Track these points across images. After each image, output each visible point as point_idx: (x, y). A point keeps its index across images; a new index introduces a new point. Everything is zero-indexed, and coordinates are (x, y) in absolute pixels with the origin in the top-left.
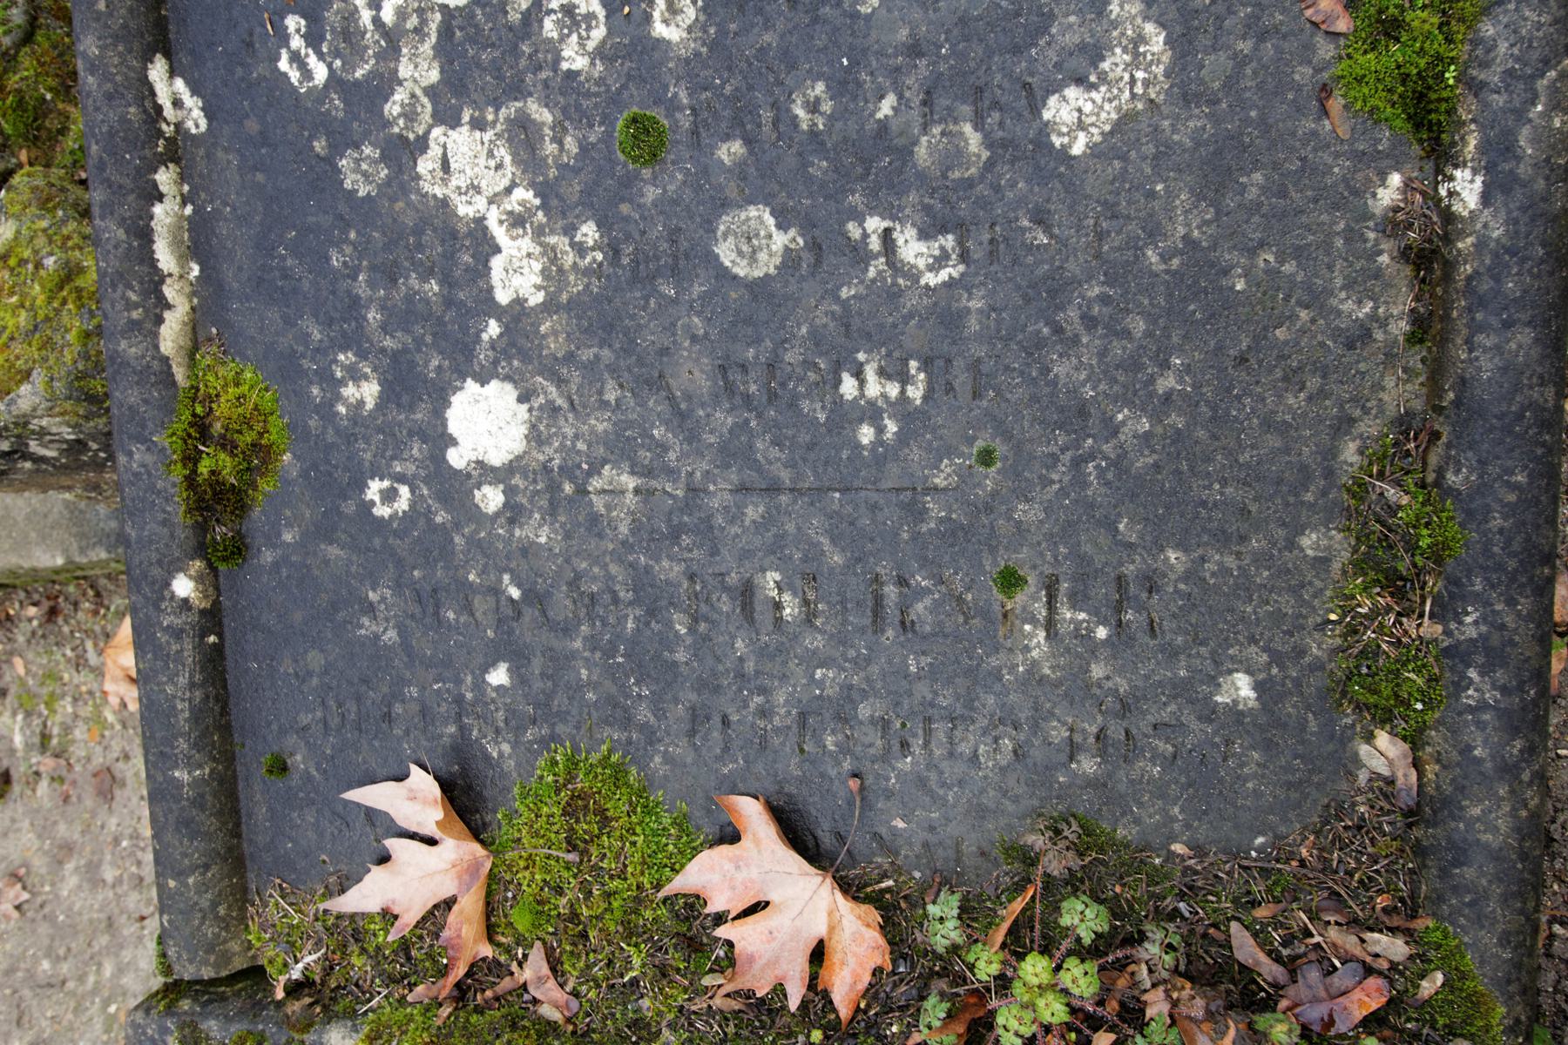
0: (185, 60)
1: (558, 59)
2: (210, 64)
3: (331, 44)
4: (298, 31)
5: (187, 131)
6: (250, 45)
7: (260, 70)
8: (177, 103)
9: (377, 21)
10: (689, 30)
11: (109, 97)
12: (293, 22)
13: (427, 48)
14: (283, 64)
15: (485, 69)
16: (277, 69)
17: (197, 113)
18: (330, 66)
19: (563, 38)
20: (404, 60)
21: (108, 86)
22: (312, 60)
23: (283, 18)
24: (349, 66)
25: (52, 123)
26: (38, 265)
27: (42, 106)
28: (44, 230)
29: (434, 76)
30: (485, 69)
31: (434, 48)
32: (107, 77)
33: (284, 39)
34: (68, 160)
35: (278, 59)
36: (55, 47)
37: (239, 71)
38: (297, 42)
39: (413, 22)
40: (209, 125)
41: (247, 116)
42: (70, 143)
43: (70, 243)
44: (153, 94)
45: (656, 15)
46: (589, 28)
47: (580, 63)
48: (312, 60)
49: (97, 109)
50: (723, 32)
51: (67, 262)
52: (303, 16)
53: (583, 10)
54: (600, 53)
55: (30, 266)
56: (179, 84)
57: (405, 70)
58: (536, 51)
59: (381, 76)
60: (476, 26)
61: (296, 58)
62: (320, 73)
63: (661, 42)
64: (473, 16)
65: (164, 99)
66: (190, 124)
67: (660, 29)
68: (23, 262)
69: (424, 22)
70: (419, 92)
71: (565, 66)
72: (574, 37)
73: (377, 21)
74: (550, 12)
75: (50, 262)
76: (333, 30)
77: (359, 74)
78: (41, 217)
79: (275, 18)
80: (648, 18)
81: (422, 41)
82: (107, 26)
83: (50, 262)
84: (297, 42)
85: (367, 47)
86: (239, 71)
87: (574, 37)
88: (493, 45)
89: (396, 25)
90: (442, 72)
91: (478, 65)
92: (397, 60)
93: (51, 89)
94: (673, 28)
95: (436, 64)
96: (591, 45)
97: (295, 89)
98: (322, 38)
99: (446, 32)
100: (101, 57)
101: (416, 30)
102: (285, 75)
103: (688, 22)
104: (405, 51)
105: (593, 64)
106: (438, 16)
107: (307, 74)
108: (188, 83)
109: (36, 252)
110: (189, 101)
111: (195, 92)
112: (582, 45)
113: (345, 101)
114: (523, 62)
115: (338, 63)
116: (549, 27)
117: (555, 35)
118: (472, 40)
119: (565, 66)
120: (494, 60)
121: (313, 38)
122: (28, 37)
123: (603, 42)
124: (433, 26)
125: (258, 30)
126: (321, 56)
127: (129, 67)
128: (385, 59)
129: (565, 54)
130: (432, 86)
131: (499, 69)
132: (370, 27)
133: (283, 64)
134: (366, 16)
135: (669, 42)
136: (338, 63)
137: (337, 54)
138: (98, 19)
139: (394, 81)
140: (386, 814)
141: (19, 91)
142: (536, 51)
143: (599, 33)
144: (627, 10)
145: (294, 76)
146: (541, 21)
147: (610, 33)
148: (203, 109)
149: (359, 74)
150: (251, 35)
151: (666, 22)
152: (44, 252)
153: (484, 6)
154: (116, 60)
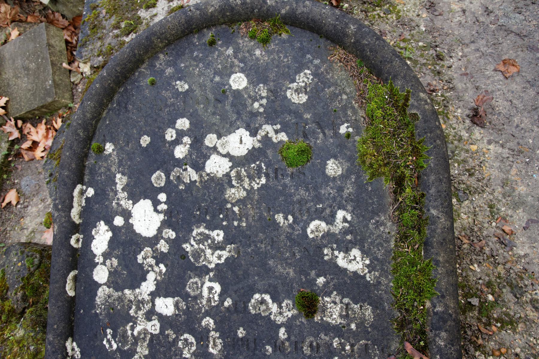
0: (77, 337)
1: (182, 354)
2: (84, 340)
3: (119, 339)
4: (110, 333)
5: (75, 357)
6: (96, 335)
7: (98, 343)
8: (73, 349)
9: (132, 334)
10: (219, 351)
11: (53, 352)
12: (109, 331)
13: (145, 344)
14: (105, 342)
15: (161, 353)
16: (103, 343)
17: (78, 353)
18: (118, 345)
19: (184, 348)
20: (139, 346)
21: (54, 349)
22: (113, 342)
23: (106, 329)
24: (123, 345)
25: (41, 290)
26: (28, 348)
27: (40, 286)
28: (32, 337)
29: (147, 352)
30: (161, 353)
31: (147, 344)
32: (53, 347)
33: (106, 335)
34: (44, 301)
35: (103, 341)
36: (46, 268)
37: (92, 342)
38: (109, 337)
39: (142, 336)
40: (81, 357)
41: (92, 356)
42: (45, 296)
43: (39, 342)
44: (66, 349)
45: (210, 346)
46: (191, 346)
47: (188, 356)
48: (113, 342)
49: (49, 355)
50: (228, 354)
51: (37, 349)
52: (112, 330)
53: (190, 341)
54: (194, 354)
55: (26, 348)
56: (74, 344)
57: (139, 349)
58: (176, 350)
59: (132, 350)
60: (160, 340)
61: (109, 341)
62: (115, 346)
63: (211, 353)
64: (159, 337)
65: (69, 350)
66: (76, 355)
67: (211, 350)
68: (24, 346)
69: (145, 337)
70: (142, 356)
71: (184, 356)
72: (187, 348)
73: (132, 334)
74: (181, 340)
75: (32, 348)
76: (120, 335)
77: (126, 348)
78: (32, 332)
79: (104, 329)
80: (208, 346)
81: (144, 342)
82: (56, 332)
83: (32, 348)
84: (109, 337)
85: (129, 341)
86: (92, 342)
87: (187, 348)
88: (164, 347)
89: (138, 336)
90: (149, 352)
91: (159, 351)
92: (137, 346)
93: (42, 281)
94: (215, 350)
95: (148, 349)
96: (191, 351)
97: (107, 350)
98: (117, 337)
99: (151, 340)
100: (53, 341)
101: (143, 338)
102: (105, 345)
103: (219, 349)
104: (139, 344)
105: (192, 357)
106: (149, 336)
107: (111, 346)
108: (77, 344)
109: (28, 344)
110: (76, 349)
111: (78, 347)
112: (189, 351)
113: (121, 355)
114: (172, 353)
115: (120, 344)
116: (180, 344)
117: (182, 347)
118: (158, 344)
119: (184, 356)
120: (164, 351)
121: (114, 336)
122: (39, 267)
123: (195, 351)
124: (148, 338)
125: (99, 331)
126: (116, 342)
127: (60, 344)
128: (133, 345)
129: (184, 352)
130: (146, 355)
131: (165, 354)
132: (130, 336)
133: (105, 342)
134: (129, 332)
135: (213, 354)
136: (120, 344)
137: (120, 342)
138: (54, 330)
139: (135, 352)
140: (140, 234)
141: (33, 284)
142: (176, 350)
143: (194, 348)
144: (202, 343)
145: (107, 346)
146: (178, 342)
147: (197, 349)
148: (80, 352)
149: (126, 348)
150: (97, 332)
151: (212, 348)
152: (31, 344)
153: (162, 335)
154: (57, 342)
